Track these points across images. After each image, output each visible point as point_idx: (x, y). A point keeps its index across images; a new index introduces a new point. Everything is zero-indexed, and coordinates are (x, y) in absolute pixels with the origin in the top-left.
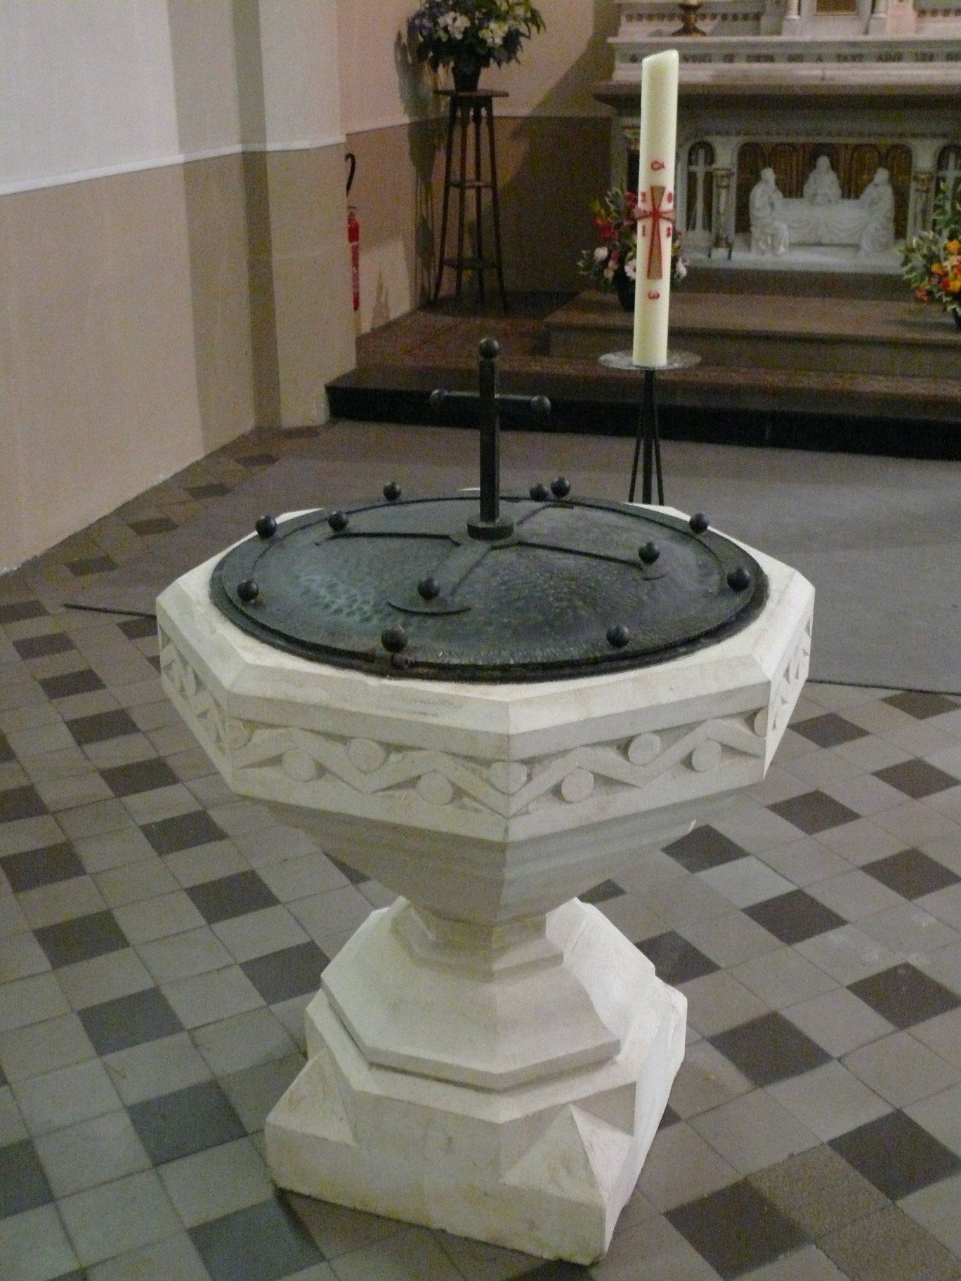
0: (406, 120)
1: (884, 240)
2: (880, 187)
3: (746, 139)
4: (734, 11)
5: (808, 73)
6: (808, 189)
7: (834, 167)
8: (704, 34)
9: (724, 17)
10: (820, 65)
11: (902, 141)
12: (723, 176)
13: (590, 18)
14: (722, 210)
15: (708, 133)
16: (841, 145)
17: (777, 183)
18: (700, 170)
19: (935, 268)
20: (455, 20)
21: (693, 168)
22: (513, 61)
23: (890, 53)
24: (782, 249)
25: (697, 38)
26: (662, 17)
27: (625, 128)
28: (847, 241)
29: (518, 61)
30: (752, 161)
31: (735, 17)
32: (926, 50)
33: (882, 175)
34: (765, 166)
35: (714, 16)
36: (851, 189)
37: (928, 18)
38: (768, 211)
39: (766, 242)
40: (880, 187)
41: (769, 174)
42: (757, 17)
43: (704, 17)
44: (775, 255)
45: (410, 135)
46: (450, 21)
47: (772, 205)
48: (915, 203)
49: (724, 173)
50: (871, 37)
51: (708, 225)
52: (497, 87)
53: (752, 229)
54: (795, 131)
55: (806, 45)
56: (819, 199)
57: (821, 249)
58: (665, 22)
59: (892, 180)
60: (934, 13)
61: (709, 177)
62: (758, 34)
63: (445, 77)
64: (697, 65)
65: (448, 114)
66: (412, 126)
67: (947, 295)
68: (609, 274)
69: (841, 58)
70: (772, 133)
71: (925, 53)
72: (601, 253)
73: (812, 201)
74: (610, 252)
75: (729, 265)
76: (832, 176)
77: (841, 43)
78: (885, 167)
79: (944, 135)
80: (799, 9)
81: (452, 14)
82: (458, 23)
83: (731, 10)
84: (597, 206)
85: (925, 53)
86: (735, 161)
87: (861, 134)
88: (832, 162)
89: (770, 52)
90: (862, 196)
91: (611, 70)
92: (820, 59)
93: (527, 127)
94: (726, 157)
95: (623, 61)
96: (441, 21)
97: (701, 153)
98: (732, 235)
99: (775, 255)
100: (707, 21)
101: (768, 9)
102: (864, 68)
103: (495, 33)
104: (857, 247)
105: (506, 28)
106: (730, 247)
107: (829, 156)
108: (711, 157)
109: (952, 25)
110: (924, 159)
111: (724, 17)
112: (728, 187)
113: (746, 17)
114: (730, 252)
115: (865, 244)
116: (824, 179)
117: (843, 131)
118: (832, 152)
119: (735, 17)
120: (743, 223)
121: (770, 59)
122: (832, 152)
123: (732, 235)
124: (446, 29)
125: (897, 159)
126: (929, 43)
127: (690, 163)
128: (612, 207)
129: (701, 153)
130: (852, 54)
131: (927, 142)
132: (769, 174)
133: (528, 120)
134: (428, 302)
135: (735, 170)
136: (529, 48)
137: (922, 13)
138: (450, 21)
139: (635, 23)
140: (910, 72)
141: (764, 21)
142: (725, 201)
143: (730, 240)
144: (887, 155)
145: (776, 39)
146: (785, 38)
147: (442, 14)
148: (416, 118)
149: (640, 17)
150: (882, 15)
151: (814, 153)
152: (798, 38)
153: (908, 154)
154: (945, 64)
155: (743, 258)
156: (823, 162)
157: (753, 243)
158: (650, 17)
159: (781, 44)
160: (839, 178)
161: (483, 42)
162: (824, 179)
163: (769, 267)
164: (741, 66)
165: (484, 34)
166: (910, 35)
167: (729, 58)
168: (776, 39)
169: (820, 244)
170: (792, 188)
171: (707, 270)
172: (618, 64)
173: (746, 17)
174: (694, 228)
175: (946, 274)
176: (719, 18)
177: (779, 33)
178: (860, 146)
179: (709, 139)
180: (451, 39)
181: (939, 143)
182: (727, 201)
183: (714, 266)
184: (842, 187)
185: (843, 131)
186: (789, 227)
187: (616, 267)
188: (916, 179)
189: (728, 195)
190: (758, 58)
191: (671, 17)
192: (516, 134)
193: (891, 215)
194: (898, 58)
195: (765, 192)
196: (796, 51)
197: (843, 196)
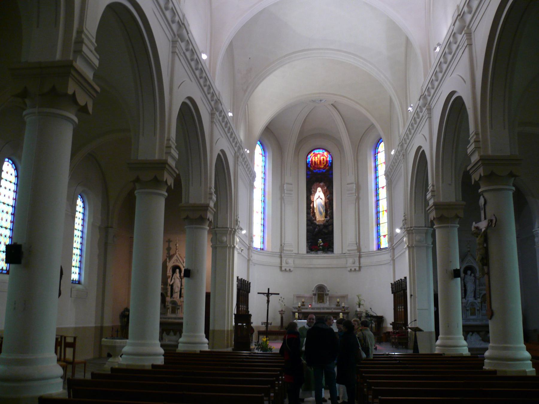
5: (170, 320)
116: (172, 333)
130: (175, 318)
132: (165, 333)
162: (172, 333)
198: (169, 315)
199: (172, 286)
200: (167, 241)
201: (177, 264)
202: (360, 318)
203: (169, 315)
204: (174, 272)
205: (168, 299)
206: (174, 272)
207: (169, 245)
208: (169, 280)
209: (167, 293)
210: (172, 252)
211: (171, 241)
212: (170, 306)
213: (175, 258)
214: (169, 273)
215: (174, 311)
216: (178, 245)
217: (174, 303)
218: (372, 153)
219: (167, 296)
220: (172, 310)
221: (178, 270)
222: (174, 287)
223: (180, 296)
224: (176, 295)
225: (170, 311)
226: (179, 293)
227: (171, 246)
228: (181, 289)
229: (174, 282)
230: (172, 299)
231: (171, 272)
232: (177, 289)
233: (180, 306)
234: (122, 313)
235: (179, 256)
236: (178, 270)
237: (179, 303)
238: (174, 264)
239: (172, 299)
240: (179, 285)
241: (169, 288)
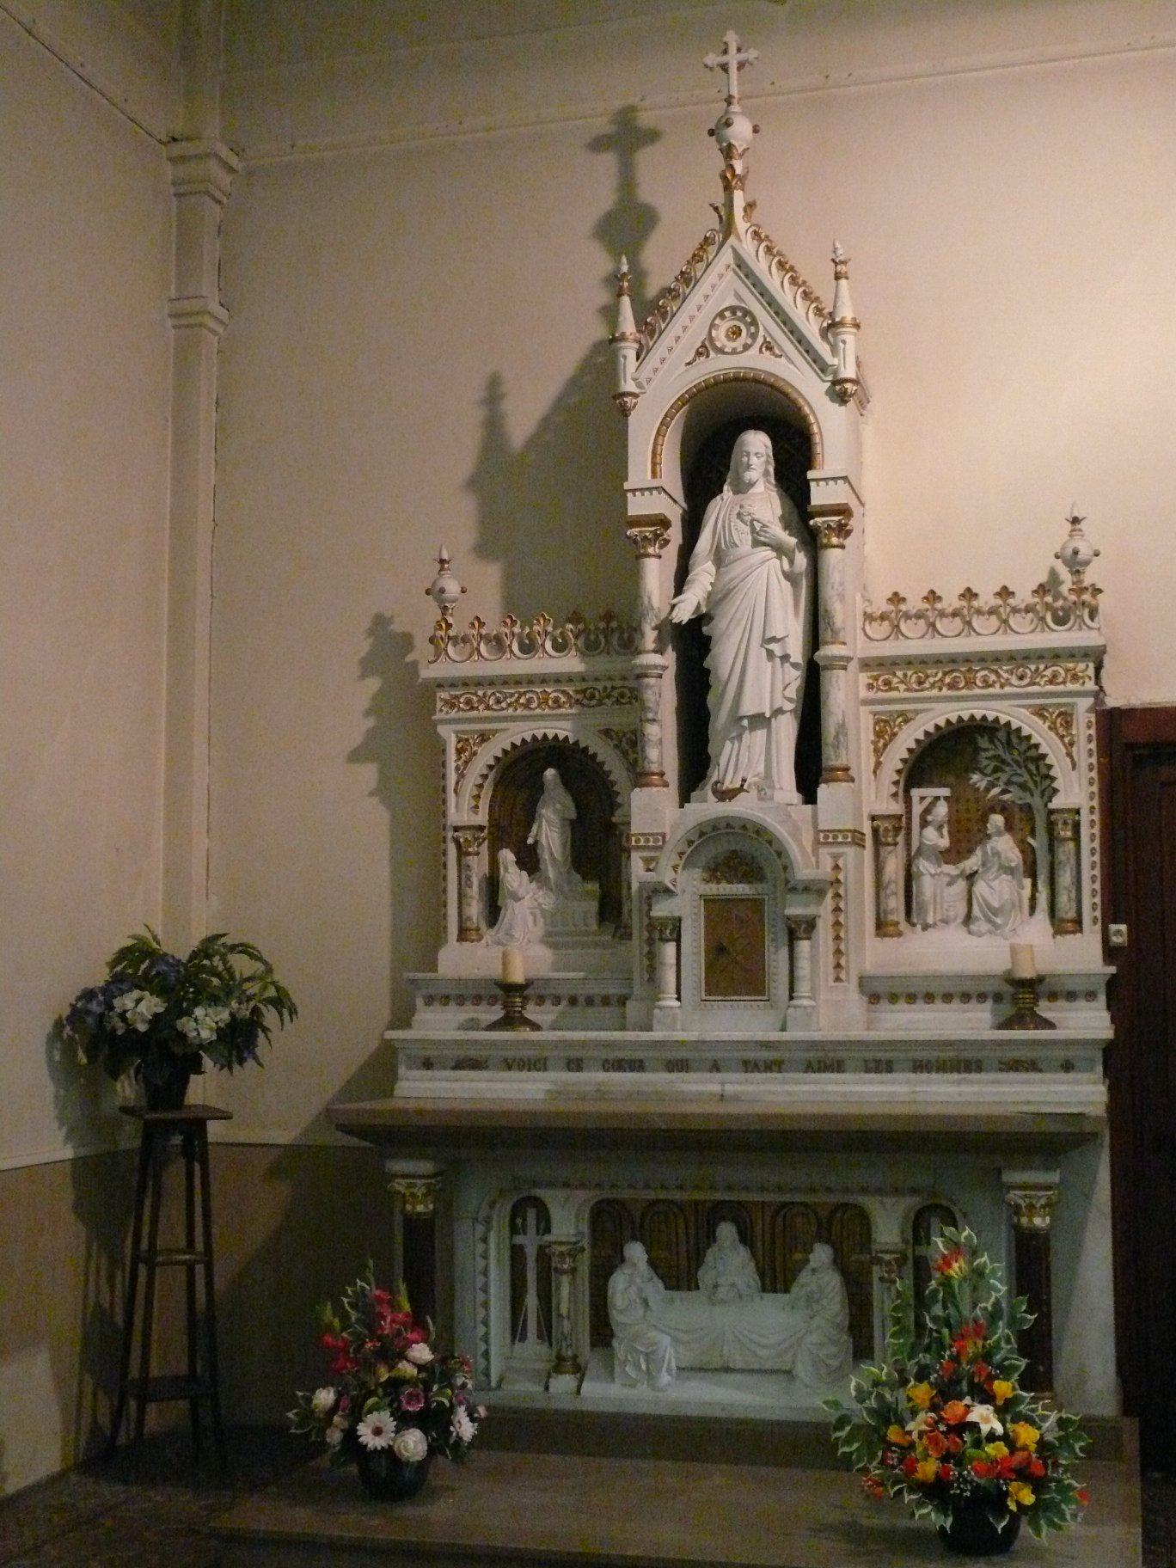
0: (68, 1153)
1: (835, 1363)
2: (820, 1273)
3: (607, 1194)
4: (604, 992)
5: (700, 1093)
6: (706, 1276)
7: (745, 1238)
8: (536, 1027)
9: (573, 1001)
10: (718, 1076)
11: (850, 1199)
12: (562, 1254)
13: (387, 1000)
14: (564, 1310)
15: (536, 1184)
16: (755, 1203)
17: (652, 1263)
18: (530, 1242)
19: (893, 1434)
20: (139, 1001)
21: (519, 1239)
22: (250, 1063)
23: (826, 1059)
24: (665, 1378)
25: (526, 1034)
26: (478, 1000)
27: (395, 1176)
28: (769, 1365)
29: (256, 1058)
30: (611, 1227)
31: (590, 1001)
32: (880, 1055)
33: (821, 1254)
34: (634, 1238)
35: (557, 1000)
36: (776, 1276)
37: (884, 1005)
38: (641, 1312)
39: (637, 1366)
40: (820, 1273)
41: (636, 1252)
42: (623, 1001)
43: (541, 1000)
44: (654, 1388)
45: (77, 1182)
46: (130, 1004)
47: (645, 1302)
48: (884, 1302)
49: (564, 1248)
50: (794, 1034)
51: (546, 1332)
52: (215, 1102)
53: (615, 1343)
54: (677, 1182)
55: (700, 1044)
56: (722, 1292)
57: (731, 1377)
58: (483, 1007)
59: (840, 1263)
60: (893, 998)
61: (543, 1256)
62: (623, 1028)
63: (126, 1089)
64: (524, 1074)
65: (137, 1143)
66: (80, 1167)
67: (911, 1490)
68: (335, 1436)
69: (749, 1066)
70: (638, 1184)
71: (880, 1059)
72: (325, 1397)
73: (712, 1301)
74: (339, 1395)
75: (579, 1405)
76: (743, 1253)
77: (745, 1044)
78: (828, 1241)
79: (914, 1191)
80: (678, 991)
81: (136, 994)
82: (142, 1008)
83: (582, 992)
84: (328, 1314)
85: (880, 1059)
86: (585, 1228)
87: (779, 1189)
88: (740, 1232)
89: (639, 1055)
90: (795, 1289)
91: (393, 1077)
92: (716, 1067)
93: (289, 1161)
94: (568, 1222)
95: (409, 1067)
96: (117, 1002)
97: (531, 1214)
98: (586, 1352)
99: (654, 1388)
100: (548, 1006)
101: (637, 990)
102: (784, 1082)
103: (204, 1023)
104: (789, 1373)
105: (225, 1016)
106: (579, 1370)
107: (735, 1221)
108: (545, 1225)
109: (920, 1016)
110: (888, 1230)
111: (573, 1001)
112: (573, 1271)
113: (606, 1001)
114: (581, 1381)
115: (803, 1370)
116: (730, 1261)
117: (757, 1183)
118: (739, 1214)
119: (590, 1001)
120: (602, 1332)
121: (638, 1066)
122: (739, 1214)
123: (586, 1352)
124: (123, 1016)
125: (846, 1232)
126: (881, 1045)
127: (514, 1230)
128: (354, 1316)
129: (531, 1214)
130: (765, 1060)
131: (889, 1201)
132: (636, 1252)
133: (293, 1152)
134: (103, 1455)
135: (585, 1243)
136: (280, 1040)
137: (874, 998)
138: (130, 1004)
139: (437, 1007)
140: (858, 1088)
141: (632, 1008)
142: (570, 1295)
143: (581, 1360)
144: (830, 1219)
145: (645, 1036)
146: (657, 1035)
147: (122, 993)
148: (82, 1152)
149: (446, 999)
150: (805, 1002)
151: (717, 1212)
152: (679, 1035)
153: (864, 1218)
154: (912, 1076)
155: (601, 1393)
156: (727, 1231)
157: (617, 1369)
158: (461, 1000)
159: (656, 1045)
160: (754, 1255)
161: (182, 1036)
162: (730, 1261)
163: (644, 1409)
164: (594, 1077)
165: (186, 1024)
166: (858, 1033)
167: (575, 1065)
168: (645, 1036)
169: (727, 1370)
170: (679, 1273)
171: (541, 1413)
172: (402, 1071)
173: (606, 1001)
174: (523, 1338)
175: (912, 1445)
176: (564, 1003)
177: (650, 1029)
178: (784, 1205)
179: (539, 1193)
180: (131, 1031)
181: (911, 1203)
182: (573, 1295)
183: (554, 1405)
184: (762, 1274)
185: (757, 1183)
186: (675, 1340)
187: (346, 1425)
188: (879, 1261)
189: (573, 1284)
190: (619, 1065)
191: (493, 1000)
192: (275, 1172)
193: (843, 1319)
194: (838, 1066)
195: (633, 1281)
196: (680, 1055)
197: (764, 1290)
198: (685, 1012)
199: (693, 642)
200: (599, 144)
201: (754, 361)
202: (631, 1275)
203: (685, 1012)
204: (706, 470)
205: (655, 811)
206: (706, 470)
207: (627, 182)
208: (656, 574)
209: (631, 744)
210: (661, 261)
211: (652, 136)
212: (686, 896)
213: (718, 287)
214: (652, 478)
215: (735, 967)
216: (741, 130)
217: (739, 854)
218: (784, 952)
219: (640, 777)
220: (717, 952)
221: (757, 446)
222: (723, 658)
223: (811, 770)
224: (758, 760)
225: (683, 961)
226: (787, 731)
227: (648, 192)
228: (813, 676)
229: (718, 598)
230: (706, 807)
231: (672, 476)
232: (758, 680)
233: (814, 890)
234: (76, 1016)
235: (762, 266)
236: (757, 446)
237: (806, 864)
238: (716, 366)
239: (706, 807)
240: (791, 628)
241: (660, 666)
